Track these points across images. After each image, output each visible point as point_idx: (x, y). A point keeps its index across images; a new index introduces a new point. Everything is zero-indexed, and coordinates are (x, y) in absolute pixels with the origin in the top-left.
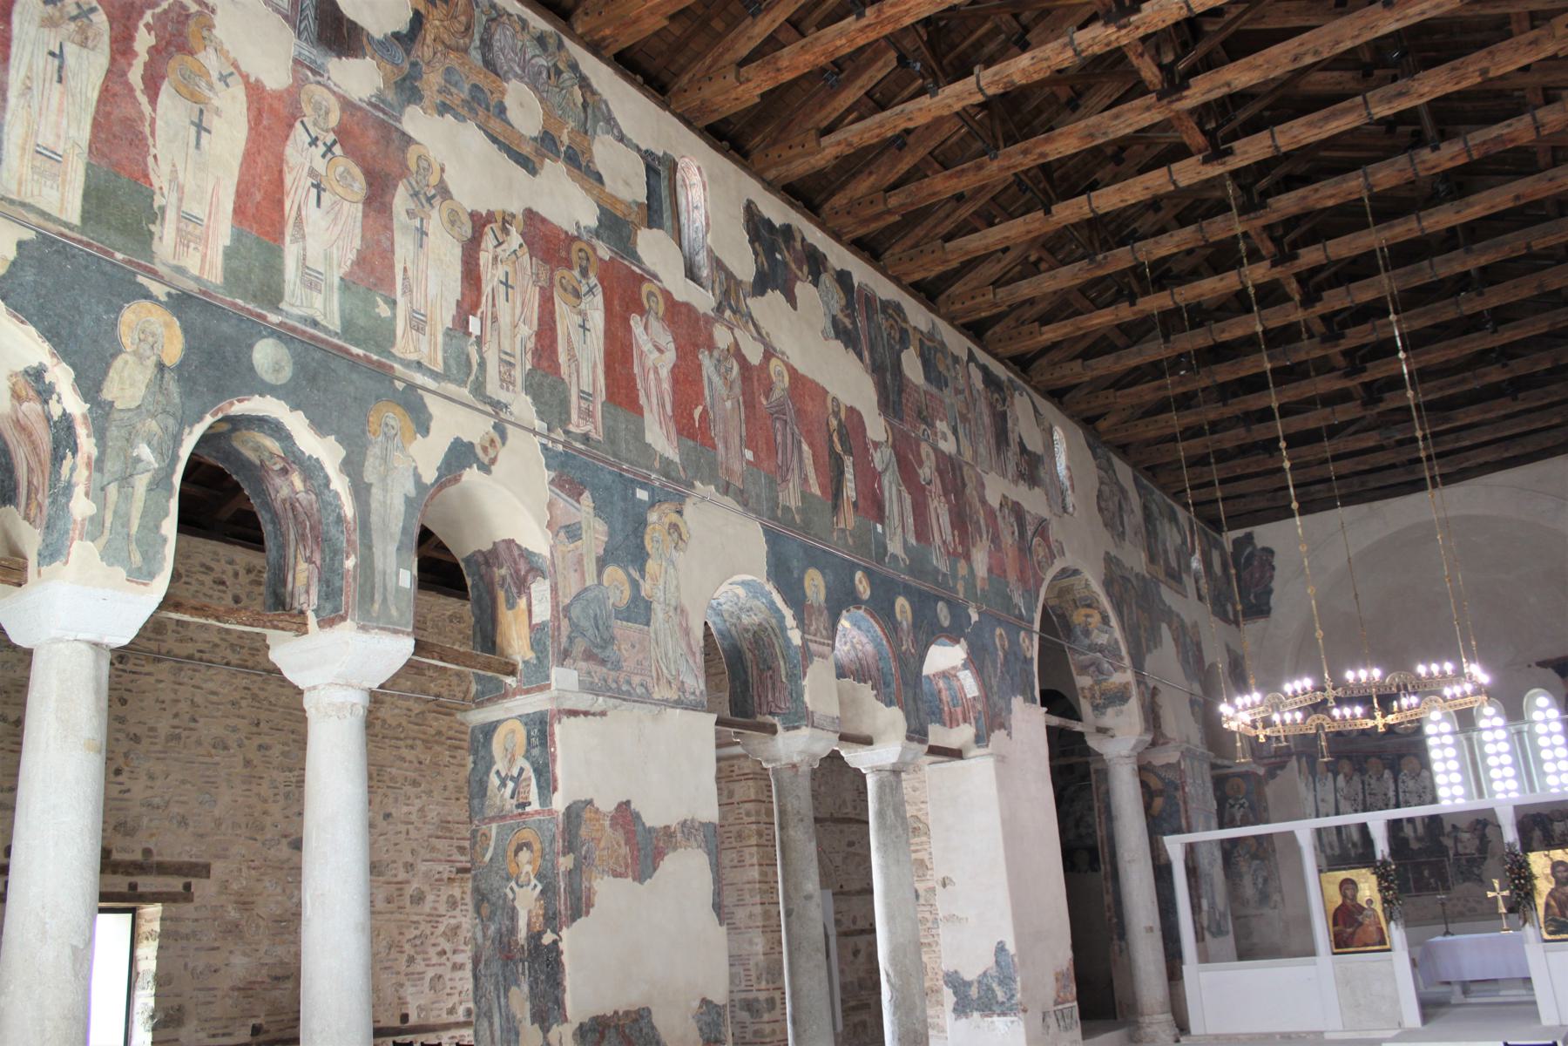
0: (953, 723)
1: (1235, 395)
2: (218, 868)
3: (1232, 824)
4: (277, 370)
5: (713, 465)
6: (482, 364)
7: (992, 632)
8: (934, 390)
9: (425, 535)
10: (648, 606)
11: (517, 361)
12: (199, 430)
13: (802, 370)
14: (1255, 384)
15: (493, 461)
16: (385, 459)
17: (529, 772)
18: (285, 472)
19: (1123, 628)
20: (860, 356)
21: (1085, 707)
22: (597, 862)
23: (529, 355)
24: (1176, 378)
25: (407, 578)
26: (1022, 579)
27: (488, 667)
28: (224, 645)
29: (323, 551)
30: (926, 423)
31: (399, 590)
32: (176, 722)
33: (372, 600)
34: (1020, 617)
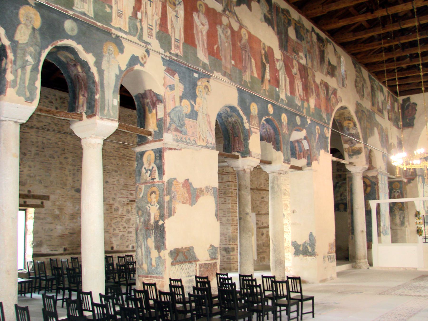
0: (300, 158)
1: (407, 48)
2: (52, 197)
3: (394, 198)
4: (72, 30)
5: (220, 65)
6: (142, 29)
7: (315, 127)
8: (299, 42)
9: (122, 86)
10: (197, 113)
11: (154, 28)
12: (47, 51)
13: (253, 33)
14: (413, 44)
15: (145, 63)
16: (109, 61)
17: (156, 168)
18: (75, 65)
19: (361, 129)
20: (273, 28)
21: (346, 155)
22: (177, 199)
23: (158, 26)
24: (386, 40)
25: (116, 102)
26: (327, 109)
27: (142, 132)
28: (53, 123)
29: (88, 93)
30: (296, 53)
31: (113, 106)
32: (37, 149)
33: (104, 109)
34: (325, 123)
